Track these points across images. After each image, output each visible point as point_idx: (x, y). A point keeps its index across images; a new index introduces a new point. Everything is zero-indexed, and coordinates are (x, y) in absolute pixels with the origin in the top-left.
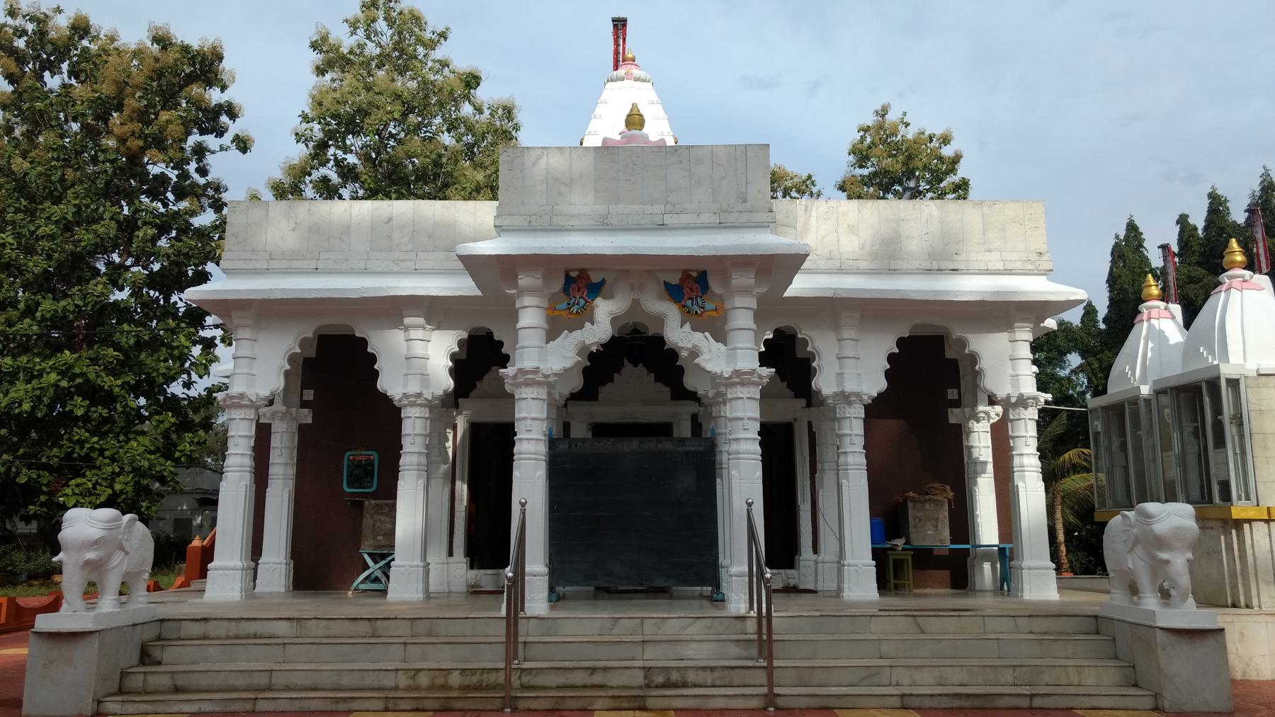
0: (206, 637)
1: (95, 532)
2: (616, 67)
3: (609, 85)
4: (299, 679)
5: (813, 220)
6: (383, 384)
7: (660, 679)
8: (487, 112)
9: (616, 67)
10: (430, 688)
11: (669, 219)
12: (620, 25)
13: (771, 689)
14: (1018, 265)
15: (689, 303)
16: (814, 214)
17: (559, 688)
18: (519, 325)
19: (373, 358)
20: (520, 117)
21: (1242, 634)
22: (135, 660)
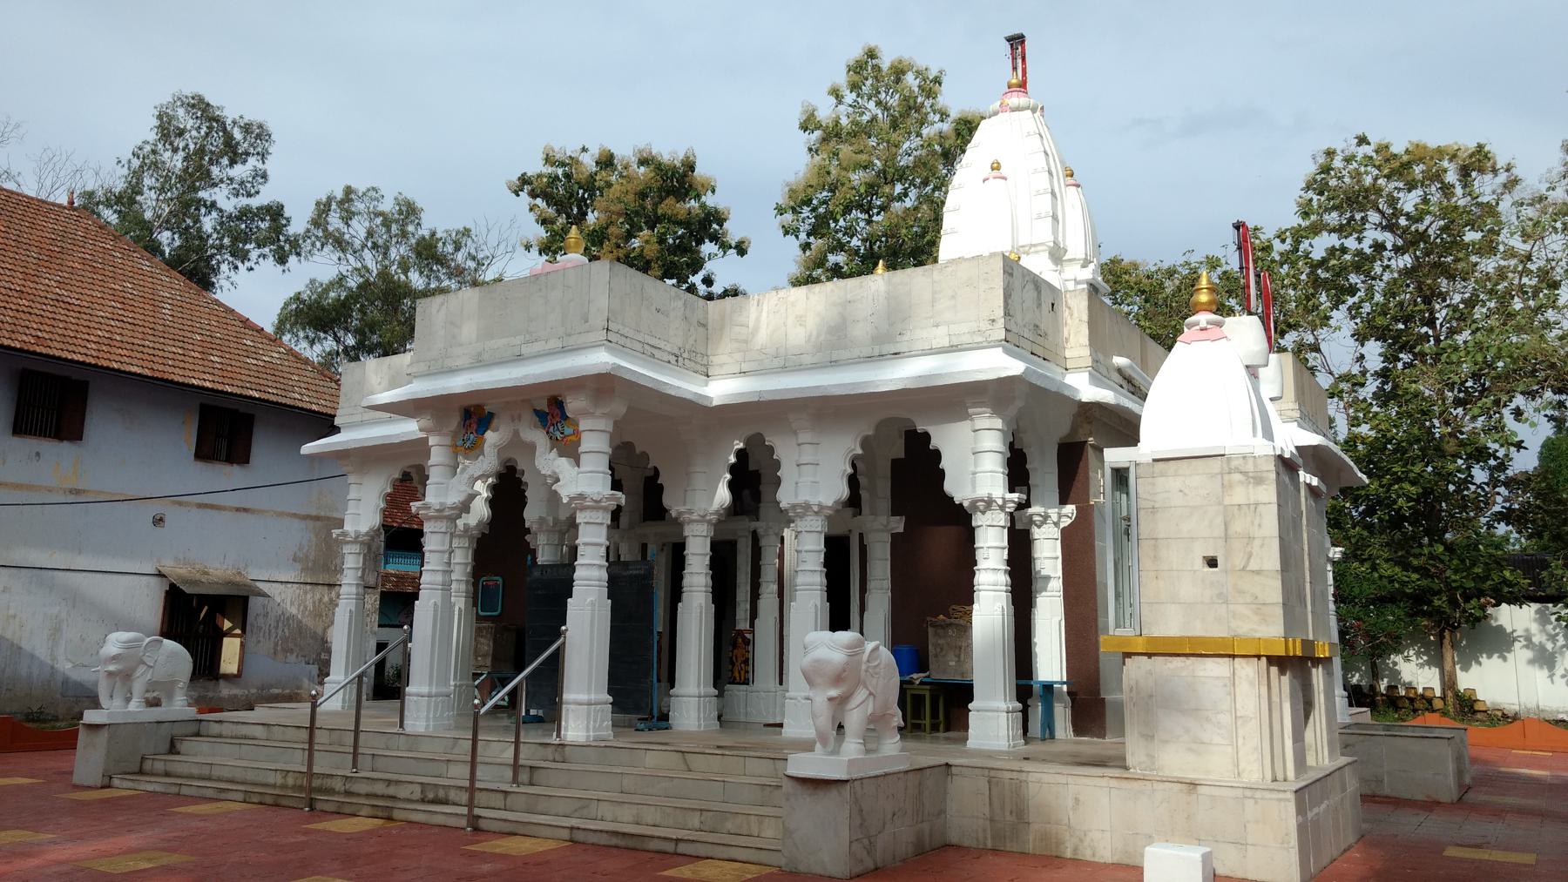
0: (220, 736)
4: (226, 773)
5: (764, 314)
6: (949, 487)
7: (431, 796)
10: (294, 788)
11: (526, 350)
13: (470, 810)
14: (966, 339)
16: (765, 308)
17: (368, 795)
18: (581, 449)
19: (937, 455)
21: (1077, 800)
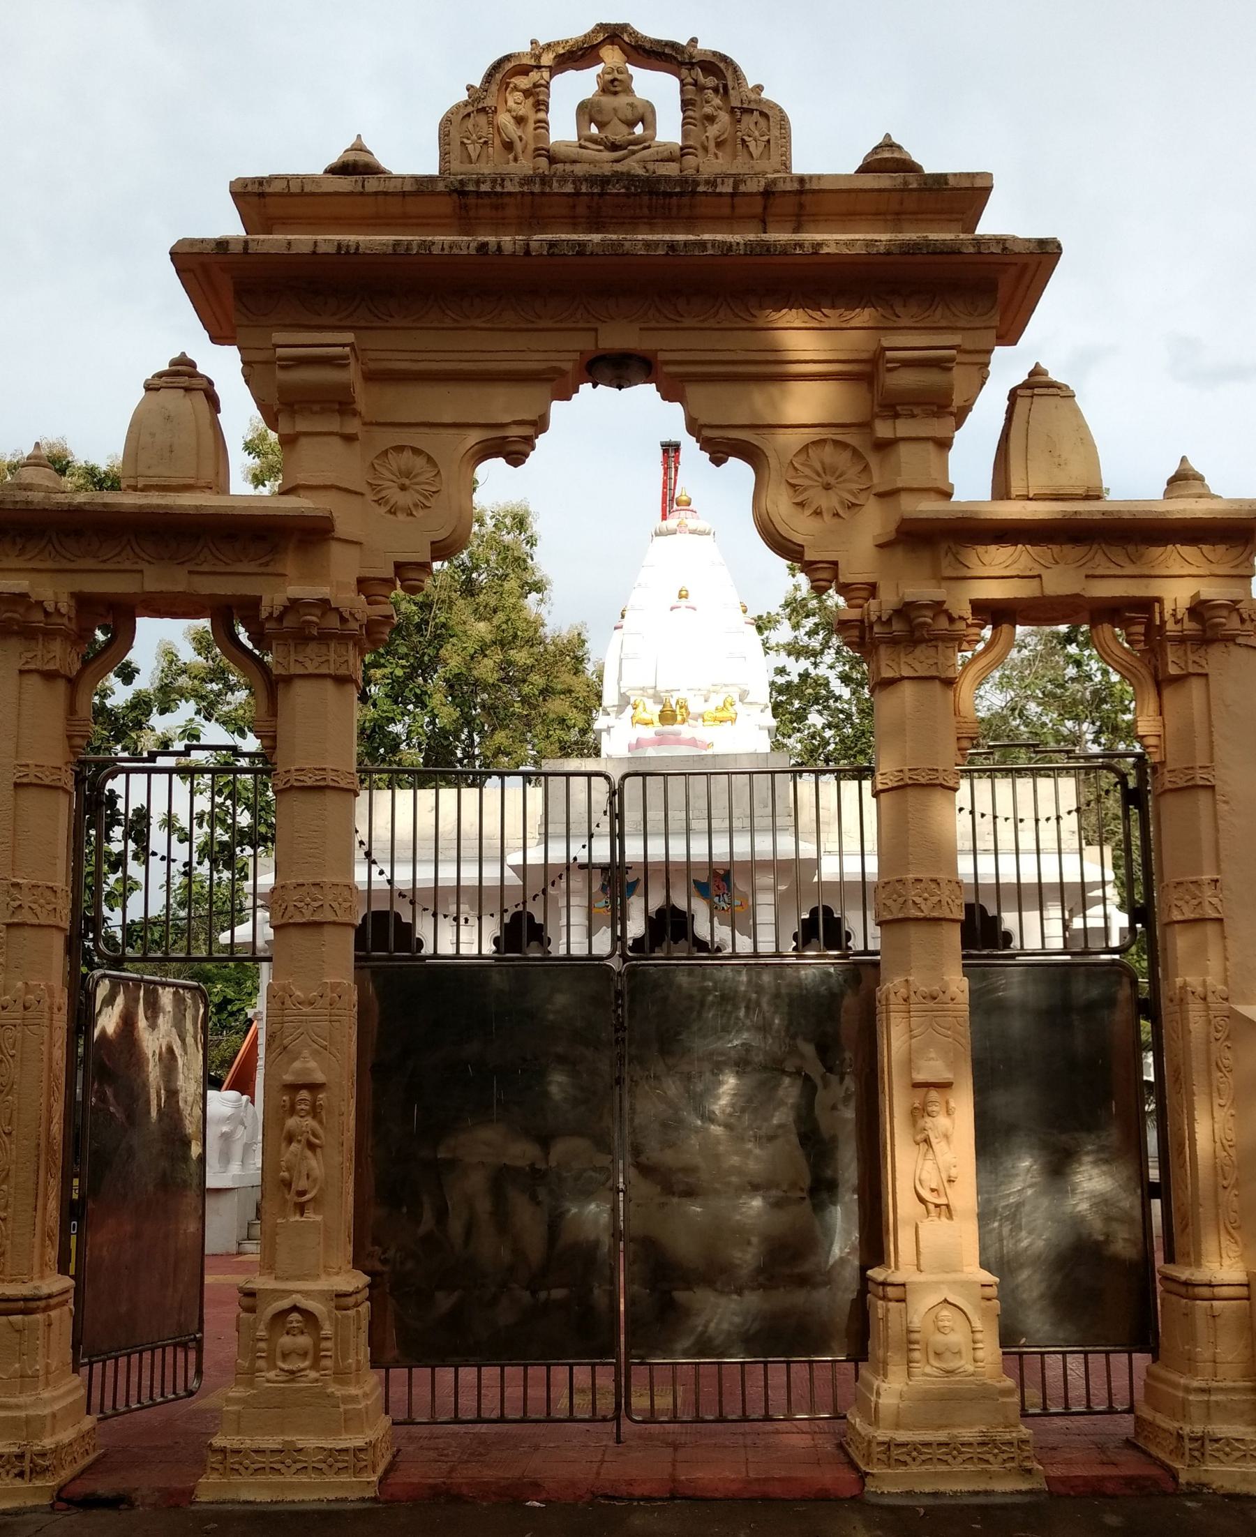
1: (228, 1111)
2: (664, 517)
8: (490, 523)
9: (664, 517)
15: (716, 899)
20: (537, 526)
22: (253, 1216)
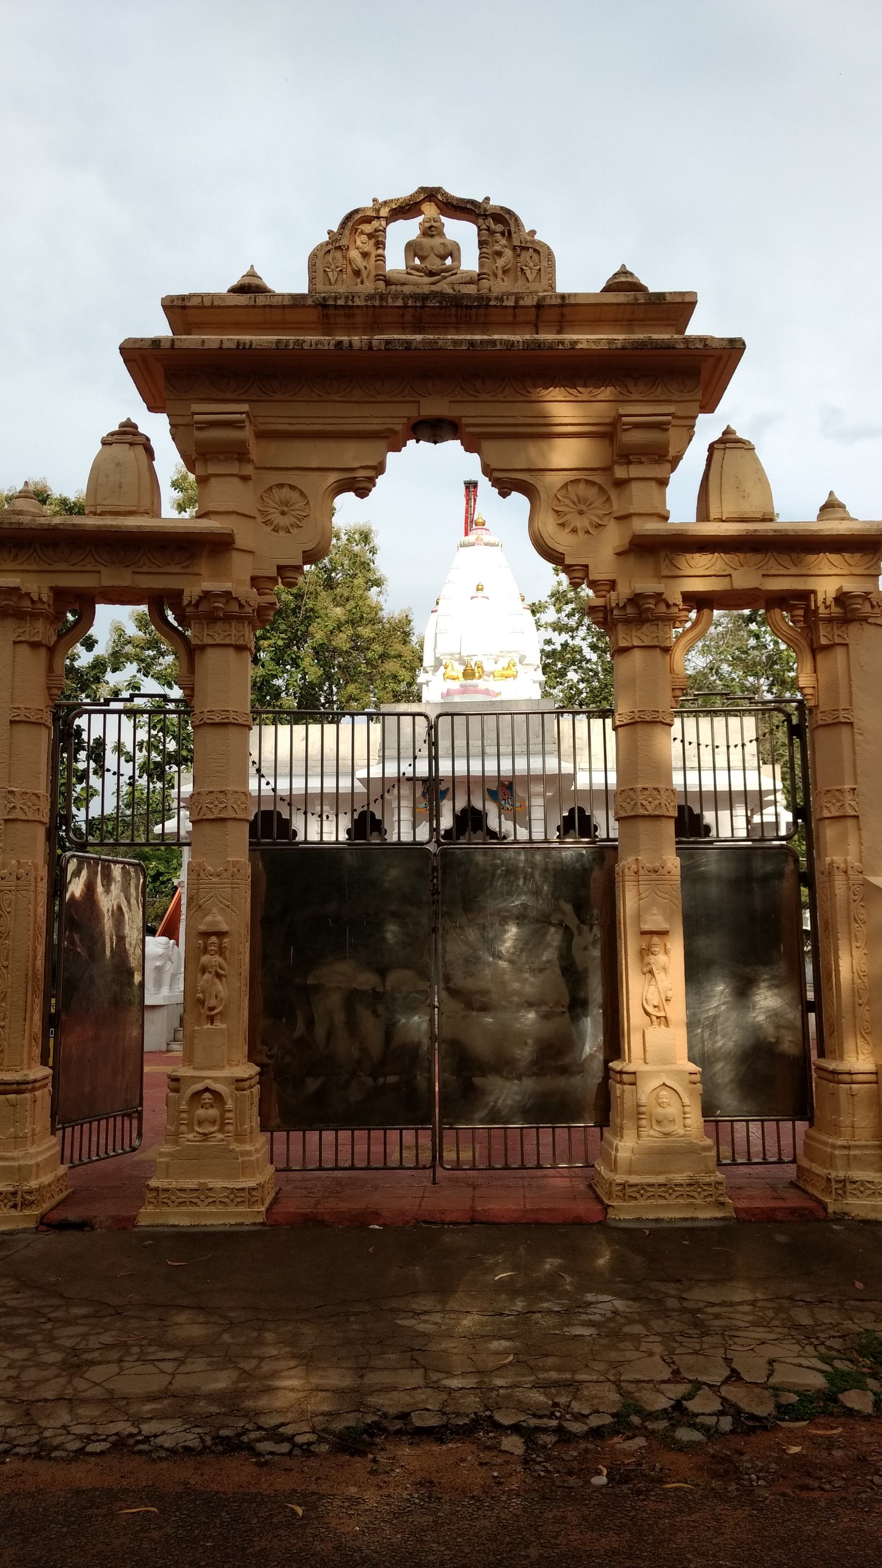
2: (466, 534)
3: (461, 549)
8: (344, 538)
9: (466, 534)
12: (472, 598)
15: (503, 802)
20: (377, 540)
